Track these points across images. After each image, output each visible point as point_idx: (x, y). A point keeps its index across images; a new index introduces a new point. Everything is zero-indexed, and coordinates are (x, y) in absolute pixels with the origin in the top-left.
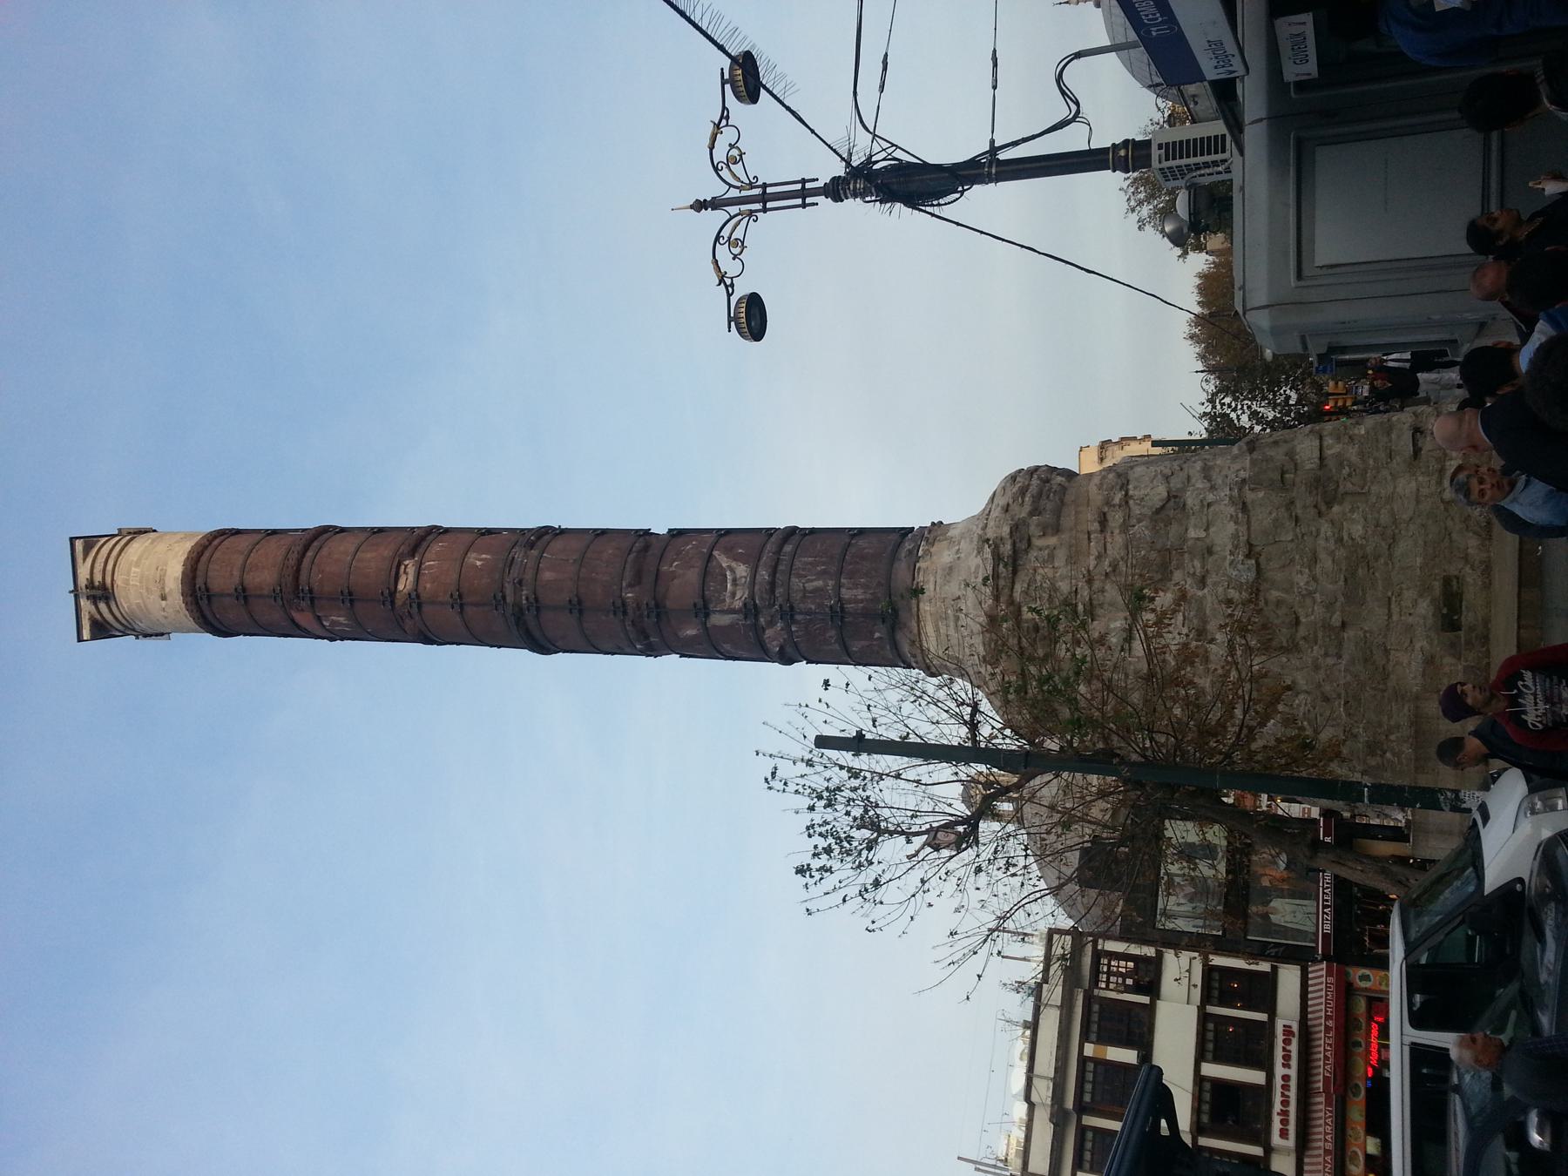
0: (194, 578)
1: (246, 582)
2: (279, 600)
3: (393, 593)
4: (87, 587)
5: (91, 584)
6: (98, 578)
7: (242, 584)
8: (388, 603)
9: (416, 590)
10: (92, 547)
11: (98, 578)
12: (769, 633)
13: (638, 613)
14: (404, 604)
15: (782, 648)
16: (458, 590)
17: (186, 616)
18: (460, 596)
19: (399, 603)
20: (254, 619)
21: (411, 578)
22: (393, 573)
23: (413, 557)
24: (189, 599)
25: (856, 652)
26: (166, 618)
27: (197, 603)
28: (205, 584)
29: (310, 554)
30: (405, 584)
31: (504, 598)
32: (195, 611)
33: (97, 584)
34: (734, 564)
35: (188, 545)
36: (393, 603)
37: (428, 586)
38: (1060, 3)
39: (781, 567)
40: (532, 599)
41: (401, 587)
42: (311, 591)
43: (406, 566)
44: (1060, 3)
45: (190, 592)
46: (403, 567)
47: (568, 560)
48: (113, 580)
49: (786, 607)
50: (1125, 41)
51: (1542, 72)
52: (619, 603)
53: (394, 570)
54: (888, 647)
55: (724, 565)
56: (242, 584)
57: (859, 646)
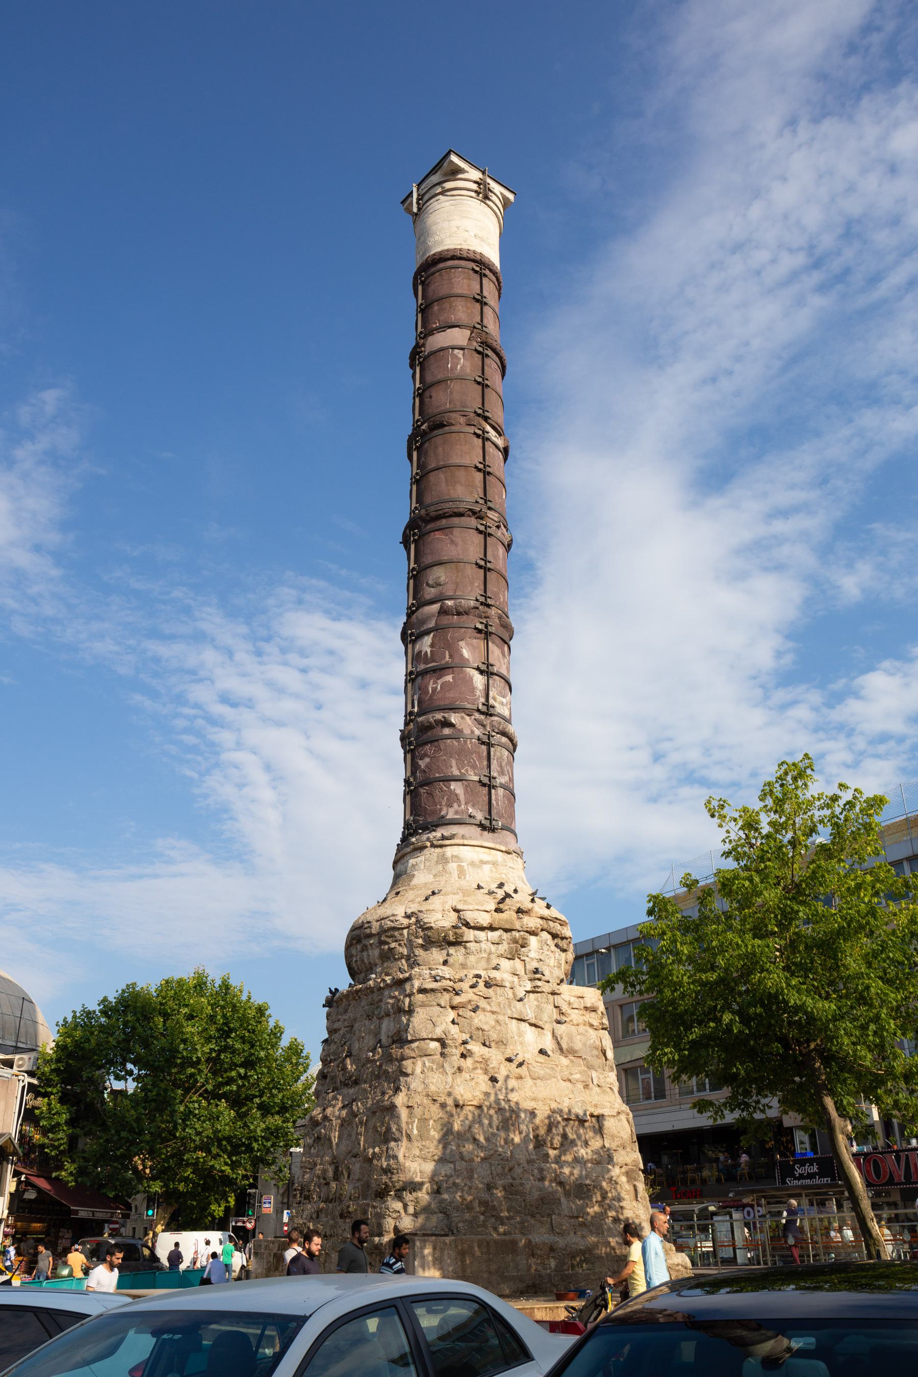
2: (479, 327)
15: (451, 725)
25: (449, 787)
52: (489, 601)
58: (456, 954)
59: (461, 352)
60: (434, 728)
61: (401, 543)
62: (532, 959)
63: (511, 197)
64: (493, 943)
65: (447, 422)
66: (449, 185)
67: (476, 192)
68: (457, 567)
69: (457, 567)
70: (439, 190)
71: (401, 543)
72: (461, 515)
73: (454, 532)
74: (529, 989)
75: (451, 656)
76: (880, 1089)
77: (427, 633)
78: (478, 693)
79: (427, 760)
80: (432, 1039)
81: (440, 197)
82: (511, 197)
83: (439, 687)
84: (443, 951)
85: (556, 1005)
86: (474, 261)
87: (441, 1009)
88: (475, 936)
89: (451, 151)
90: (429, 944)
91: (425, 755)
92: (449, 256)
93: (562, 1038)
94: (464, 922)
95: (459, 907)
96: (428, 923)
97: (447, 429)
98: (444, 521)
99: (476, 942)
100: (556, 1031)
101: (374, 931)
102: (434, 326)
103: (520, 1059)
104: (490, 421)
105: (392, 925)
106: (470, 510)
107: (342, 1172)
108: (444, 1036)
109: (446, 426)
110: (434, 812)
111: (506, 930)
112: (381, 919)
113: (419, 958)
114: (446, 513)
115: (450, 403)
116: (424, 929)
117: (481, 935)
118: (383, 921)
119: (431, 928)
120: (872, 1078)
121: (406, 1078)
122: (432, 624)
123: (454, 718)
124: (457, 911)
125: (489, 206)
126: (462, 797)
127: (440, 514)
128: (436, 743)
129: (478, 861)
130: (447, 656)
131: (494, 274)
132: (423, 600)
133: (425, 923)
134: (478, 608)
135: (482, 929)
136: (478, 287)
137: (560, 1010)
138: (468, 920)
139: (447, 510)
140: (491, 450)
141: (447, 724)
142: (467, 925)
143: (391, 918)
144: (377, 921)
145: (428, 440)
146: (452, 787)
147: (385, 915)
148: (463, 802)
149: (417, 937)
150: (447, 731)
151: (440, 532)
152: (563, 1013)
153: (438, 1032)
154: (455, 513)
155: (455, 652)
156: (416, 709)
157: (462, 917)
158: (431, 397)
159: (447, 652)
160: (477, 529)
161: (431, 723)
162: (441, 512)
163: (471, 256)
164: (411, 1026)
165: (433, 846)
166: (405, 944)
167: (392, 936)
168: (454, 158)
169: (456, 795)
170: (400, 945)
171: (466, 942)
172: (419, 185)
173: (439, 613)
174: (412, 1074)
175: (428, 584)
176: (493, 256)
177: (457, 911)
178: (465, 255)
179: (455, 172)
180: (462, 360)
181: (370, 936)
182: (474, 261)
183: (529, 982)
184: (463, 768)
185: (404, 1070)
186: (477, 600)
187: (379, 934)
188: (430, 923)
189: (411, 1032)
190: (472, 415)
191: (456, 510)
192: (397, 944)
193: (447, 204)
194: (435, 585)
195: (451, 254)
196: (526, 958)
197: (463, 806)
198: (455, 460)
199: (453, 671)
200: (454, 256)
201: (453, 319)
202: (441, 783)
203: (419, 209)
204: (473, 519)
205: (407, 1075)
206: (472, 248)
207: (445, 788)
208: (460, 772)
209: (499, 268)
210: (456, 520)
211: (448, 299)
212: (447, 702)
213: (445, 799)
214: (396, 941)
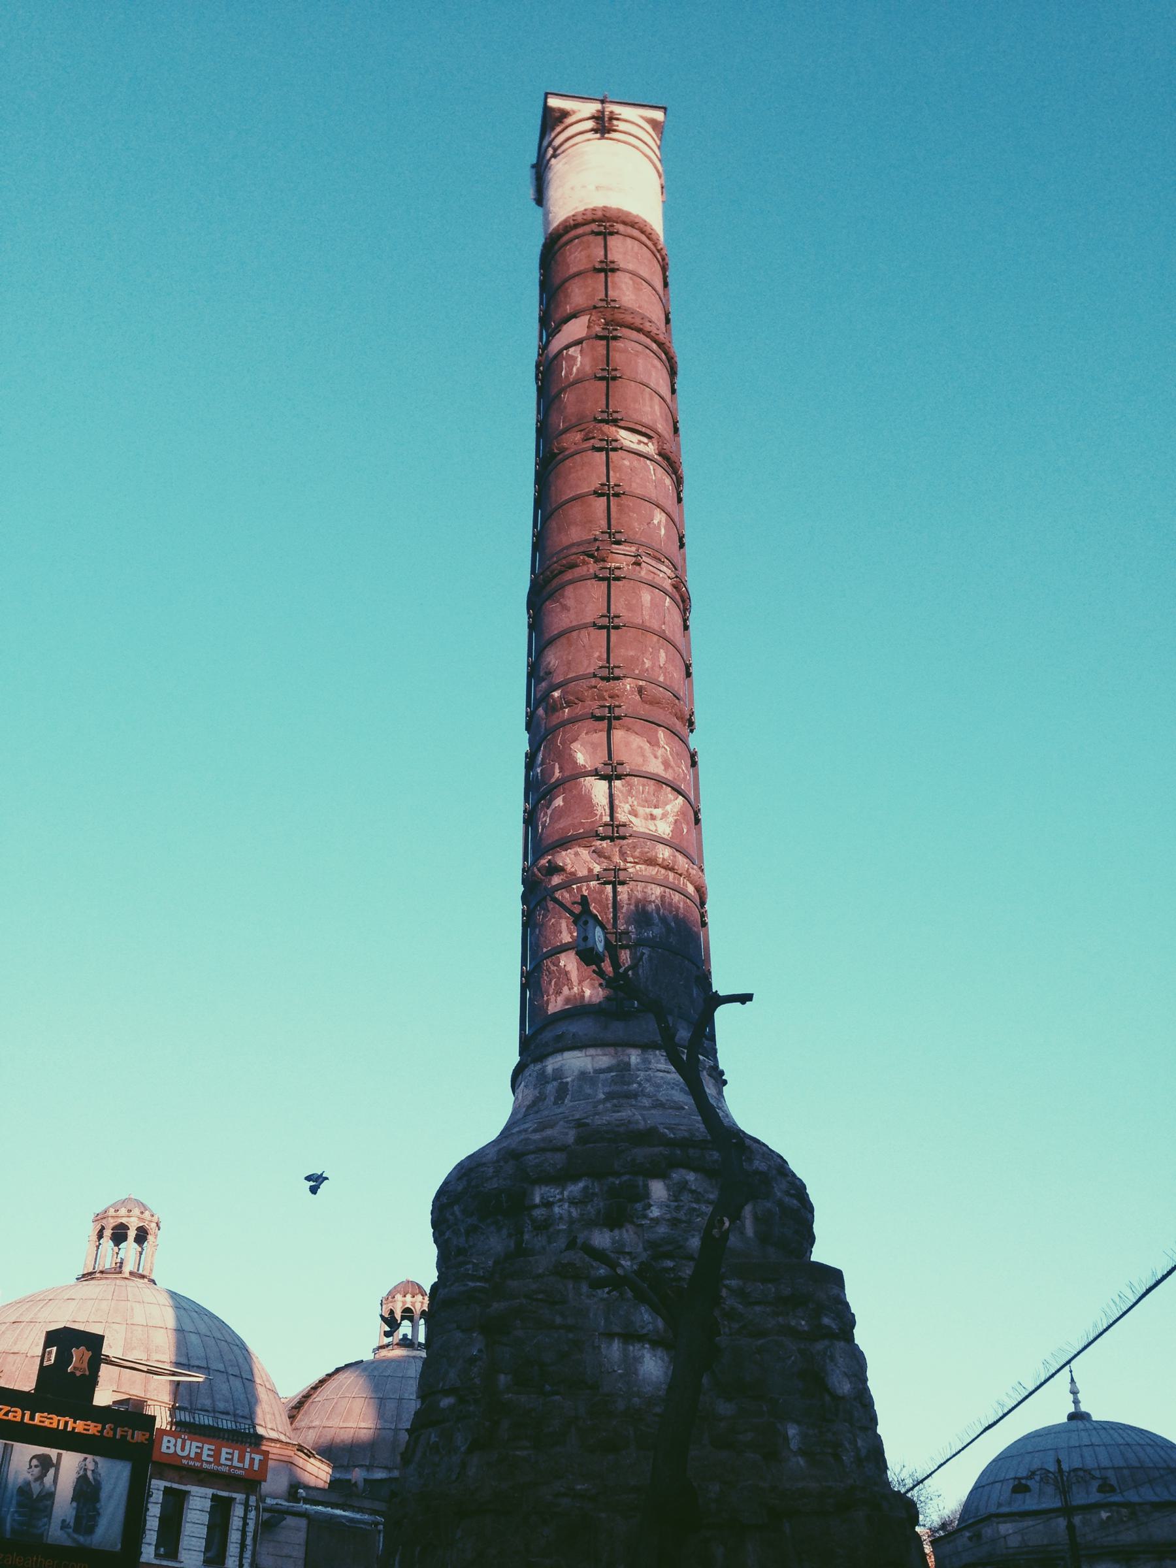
0: (624, 223)
1: (618, 273)
2: (604, 304)
3: (615, 422)
4: (611, 112)
5: (612, 117)
6: (622, 126)
7: (618, 269)
8: (605, 416)
9: (621, 449)
10: (654, 129)
11: (622, 126)
12: (584, 853)
13: (606, 695)
14: (603, 433)
16: (623, 494)
17: (576, 208)
18: (617, 495)
19: (606, 428)
20: (575, 276)
21: (635, 446)
22: (639, 428)
23: (660, 454)
24: (600, 214)
25: (557, 965)
26: (572, 188)
27: (594, 221)
28: (617, 233)
29: (654, 346)
30: (627, 439)
31: (618, 543)
32: (585, 217)
33: (615, 122)
34: (671, 819)
35: (650, 280)
36: (606, 422)
37: (627, 463)
38: (1074, 1392)
39: (671, 875)
40: (617, 573)
41: (623, 433)
42: (615, 338)
43: (646, 444)
44: (1074, 1392)
45: (608, 215)
46: (645, 440)
47: (664, 624)
48: (619, 141)
49: (622, 876)
50: (159, 1506)
51: (183, 1419)
52: (617, 672)
53: (644, 430)
54: (496, 1149)
55: (669, 808)
56: (618, 269)
57: (568, 969)
59: (578, 348)
62: (656, 1221)
63: (659, 115)
78: (600, 811)
82: (659, 115)
83: (548, 820)
89: (547, 95)
103: (133, 1224)
104: (621, 424)
120: (723, 1306)
125: (619, 141)
126: (574, 976)
129: (591, 1071)
131: (633, 226)
136: (602, 253)
140: (627, 463)
146: (562, 964)
148: (575, 982)
155: (566, 758)
159: (557, 766)
163: (589, 216)
169: (567, 973)
176: (655, 220)
180: (579, 359)
197: (576, 989)
206: (591, 206)
209: (662, 238)
212: (556, 837)
213: (553, 983)
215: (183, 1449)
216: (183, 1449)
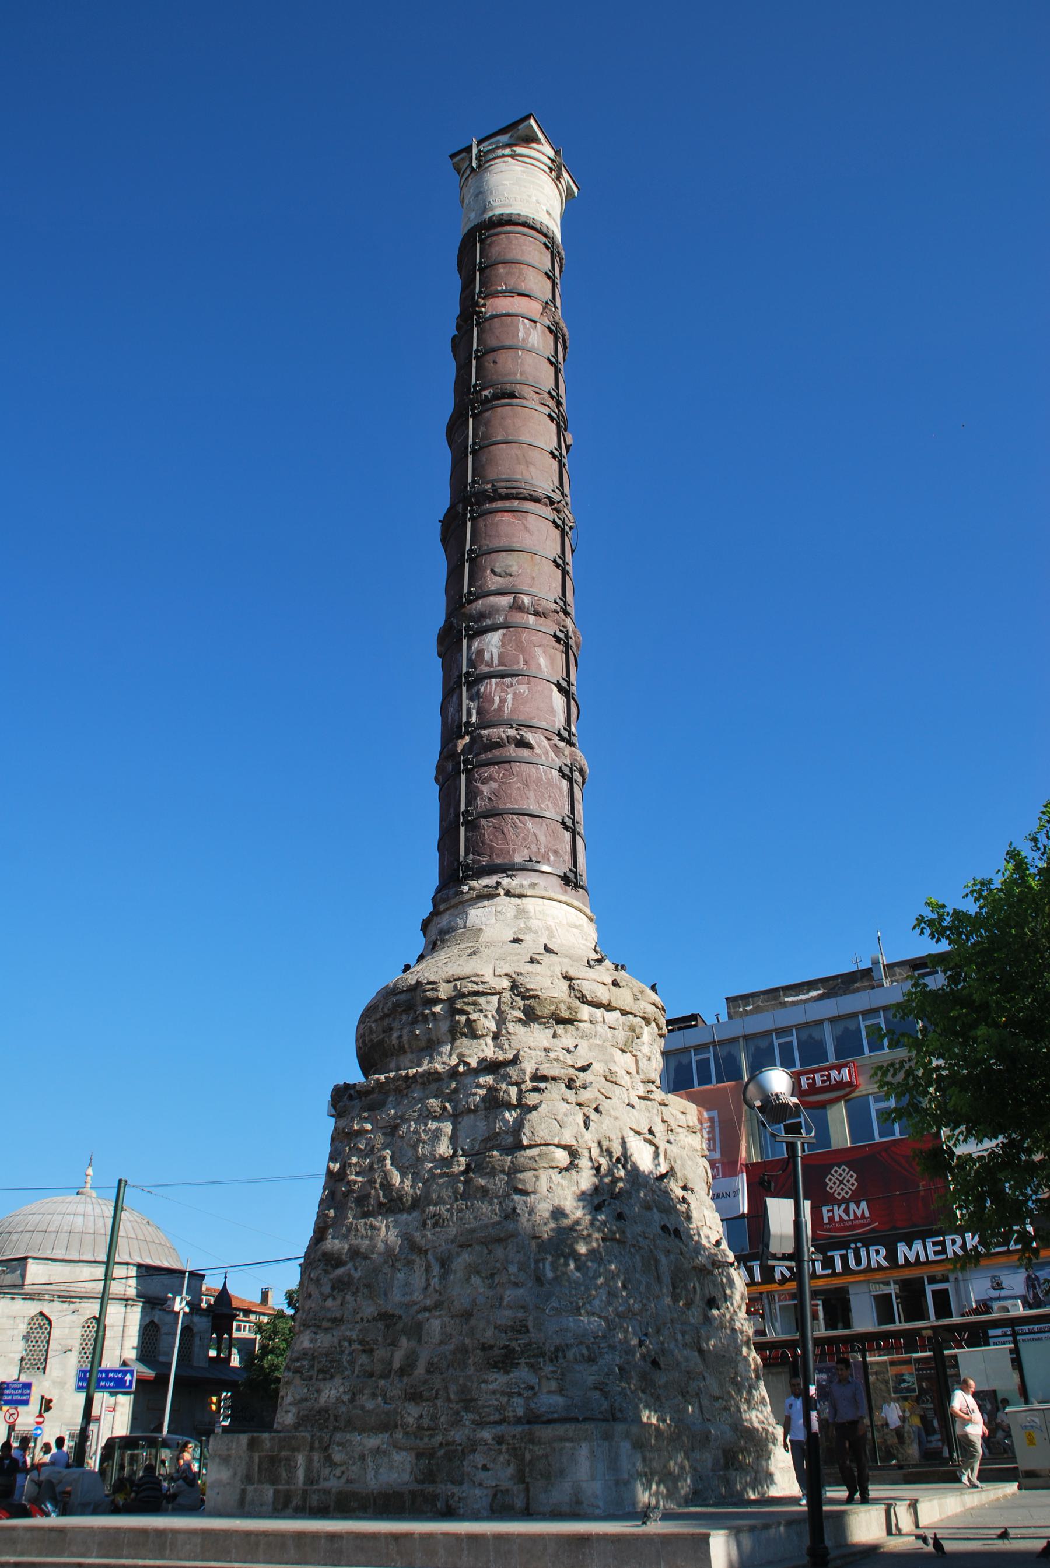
15: (528, 746)
58: (567, 1037)
60: (505, 746)
61: (440, 521)
64: (610, 1028)
65: (520, 394)
66: (519, 150)
67: (550, 168)
68: (532, 557)
69: (532, 557)
70: (508, 151)
71: (440, 521)
72: (537, 500)
73: (529, 519)
74: (641, 1093)
75: (526, 663)
76: (409, 1340)
77: (493, 628)
79: (494, 785)
80: (558, 1146)
81: (509, 159)
84: (547, 1030)
85: (665, 1119)
86: (546, 236)
87: (567, 1105)
88: (591, 1015)
90: (530, 1017)
91: (491, 778)
92: (520, 221)
93: (675, 1162)
94: (578, 995)
95: (572, 973)
96: (532, 990)
97: (515, 401)
98: (516, 503)
99: (591, 1022)
100: (668, 1151)
101: (443, 996)
102: (499, 288)
105: (476, 988)
106: (549, 497)
107: (742, 1298)
108: (574, 1143)
109: (517, 397)
110: (503, 852)
111: (624, 1013)
112: (455, 980)
113: (513, 1037)
114: (521, 494)
115: (521, 374)
116: (524, 998)
117: (599, 1013)
118: (458, 983)
119: (535, 997)
121: (524, 1198)
122: (501, 619)
123: (530, 737)
124: (567, 978)
127: (513, 494)
128: (507, 766)
130: (522, 662)
132: (486, 589)
133: (528, 990)
134: (558, 613)
135: (597, 1005)
137: (669, 1125)
138: (585, 992)
139: (522, 490)
141: (522, 743)
142: (583, 999)
143: (474, 979)
144: (449, 982)
145: (492, 409)
147: (462, 974)
149: (513, 1008)
150: (525, 753)
151: (510, 514)
152: (672, 1131)
153: (568, 1139)
154: (531, 496)
156: (474, 720)
157: (576, 987)
158: (495, 362)
160: (554, 522)
161: (502, 739)
162: (514, 491)
163: (545, 230)
164: (527, 1125)
165: (508, 894)
166: (493, 1016)
167: (474, 1004)
168: (532, 122)
170: (486, 1016)
171: (580, 1021)
172: (479, 143)
173: (510, 607)
174: (534, 1193)
175: (493, 571)
177: (567, 978)
178: (538, 226)
179: (530, 139)
181: (437, 1001)
182: (546, 236)
183: (642, 1084)
184: (543, 802)
185: (520, 1186)
186: (556, 602)
187: (451, 1000)
188: (536, 990)
189: (528, 1134)
190: (546, 395)
191: (533, 493)
192: (482, 1015)
193: (519, 168)
194: (503, 574)
195: (524, 220)
196: (638, 1053)
198: (523, 438)
199: (529, 680)
200: (526, 222)
201: (523, 287)
202: (515, 817)
203: (479, 166)
204: (549, 508)
205: (525, 1193)
207: (519, 824)
208: (540, 806)
210: (529, 506)
211: (518, 265)
214: (481, 1011)
215: (858, 1262)
216: (858, 1262)
